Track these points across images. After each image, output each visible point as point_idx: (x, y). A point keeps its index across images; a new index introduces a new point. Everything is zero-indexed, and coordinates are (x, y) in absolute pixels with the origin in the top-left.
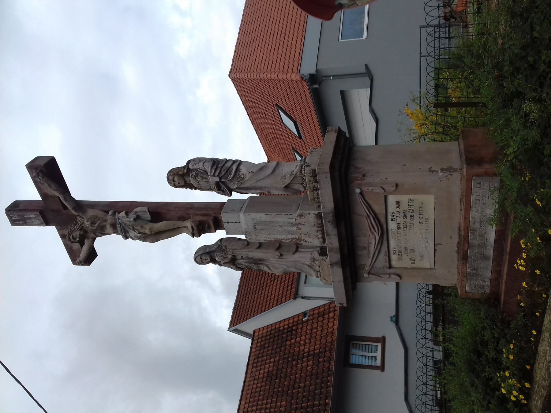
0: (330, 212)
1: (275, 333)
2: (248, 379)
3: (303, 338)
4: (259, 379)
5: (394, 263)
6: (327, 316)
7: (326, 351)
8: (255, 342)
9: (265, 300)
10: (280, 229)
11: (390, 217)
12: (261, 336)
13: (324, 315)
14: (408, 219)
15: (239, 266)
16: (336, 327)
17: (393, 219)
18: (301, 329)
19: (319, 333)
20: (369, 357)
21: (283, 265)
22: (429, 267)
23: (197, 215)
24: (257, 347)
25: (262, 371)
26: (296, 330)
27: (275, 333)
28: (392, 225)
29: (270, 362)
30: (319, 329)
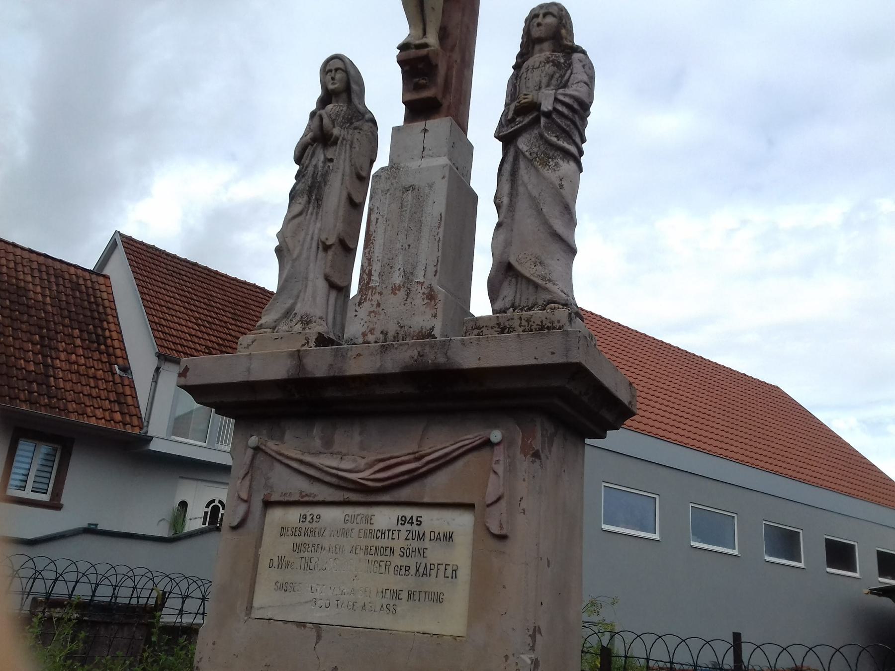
0: (448, 358)
1: (99, 313)
2: (18, 252)
3: (82, 361)
4: (16, 271)
5: (277, 515)
6: (117, 409)
7: (49, 397)
8: (87, 275)
9: (163, 303)
10: (399, 246)
11: (408, 512)
12: (97, 287)
13: (120, 403)
14: (397, 560)
15: (309, 151)
16: (93, 421)
17: (403, 520)
18: (100, 360)
19: (86, 390)
20: (26, 481)
21: (302, 249)
22: (256, 604)
23: (449, 68)
24: (78, 277)
25: (29, 278)
26: (98, 350)
27: (99, 313)
28: (385, 518)
29: (44, 296)
30: (94, 392)
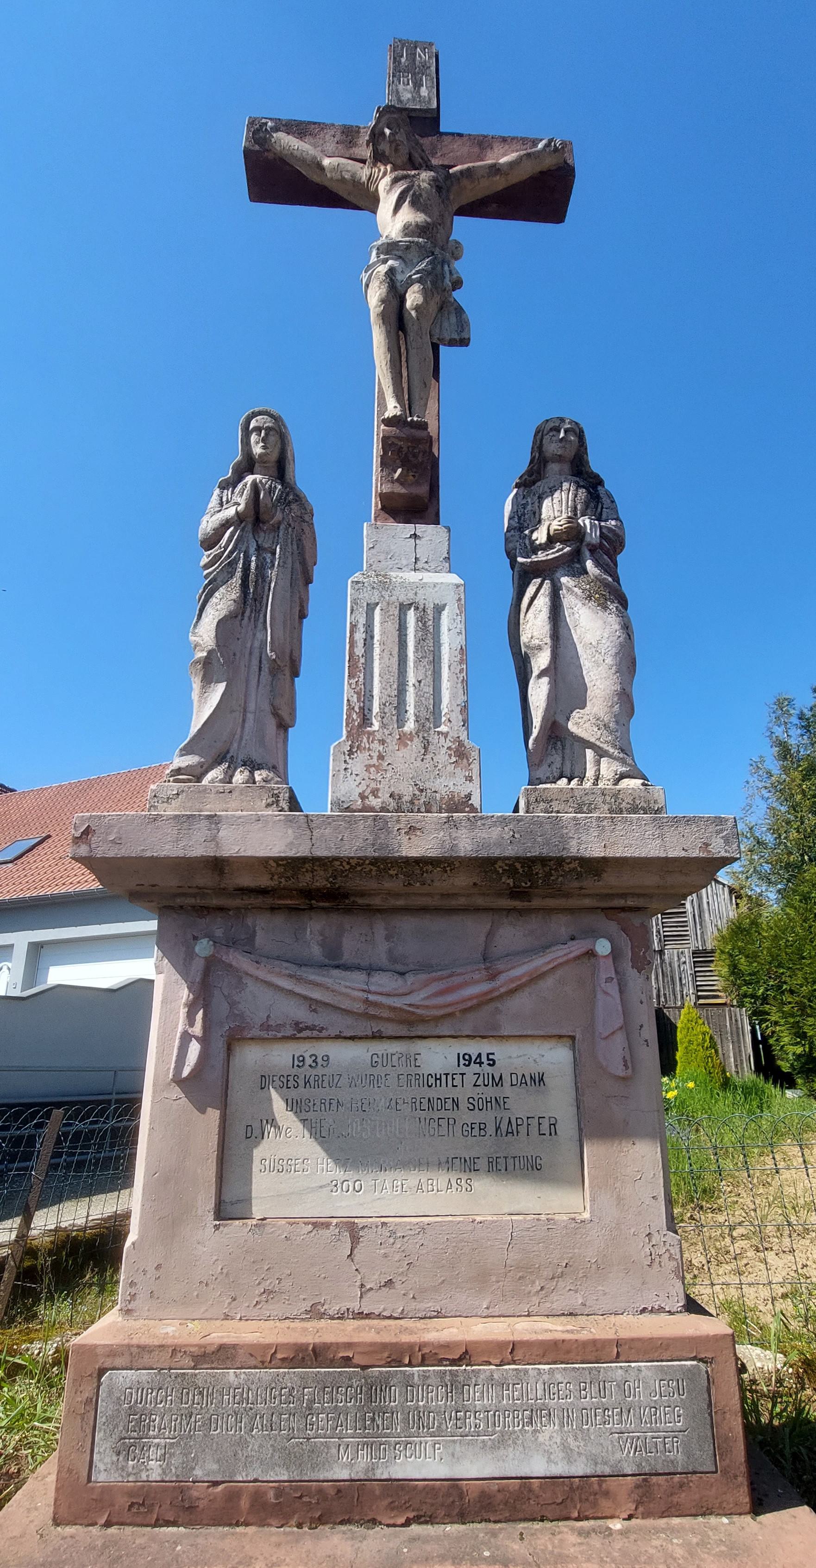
14: (465, 1116)
17: (468, 1060)
28: (437, 1056)
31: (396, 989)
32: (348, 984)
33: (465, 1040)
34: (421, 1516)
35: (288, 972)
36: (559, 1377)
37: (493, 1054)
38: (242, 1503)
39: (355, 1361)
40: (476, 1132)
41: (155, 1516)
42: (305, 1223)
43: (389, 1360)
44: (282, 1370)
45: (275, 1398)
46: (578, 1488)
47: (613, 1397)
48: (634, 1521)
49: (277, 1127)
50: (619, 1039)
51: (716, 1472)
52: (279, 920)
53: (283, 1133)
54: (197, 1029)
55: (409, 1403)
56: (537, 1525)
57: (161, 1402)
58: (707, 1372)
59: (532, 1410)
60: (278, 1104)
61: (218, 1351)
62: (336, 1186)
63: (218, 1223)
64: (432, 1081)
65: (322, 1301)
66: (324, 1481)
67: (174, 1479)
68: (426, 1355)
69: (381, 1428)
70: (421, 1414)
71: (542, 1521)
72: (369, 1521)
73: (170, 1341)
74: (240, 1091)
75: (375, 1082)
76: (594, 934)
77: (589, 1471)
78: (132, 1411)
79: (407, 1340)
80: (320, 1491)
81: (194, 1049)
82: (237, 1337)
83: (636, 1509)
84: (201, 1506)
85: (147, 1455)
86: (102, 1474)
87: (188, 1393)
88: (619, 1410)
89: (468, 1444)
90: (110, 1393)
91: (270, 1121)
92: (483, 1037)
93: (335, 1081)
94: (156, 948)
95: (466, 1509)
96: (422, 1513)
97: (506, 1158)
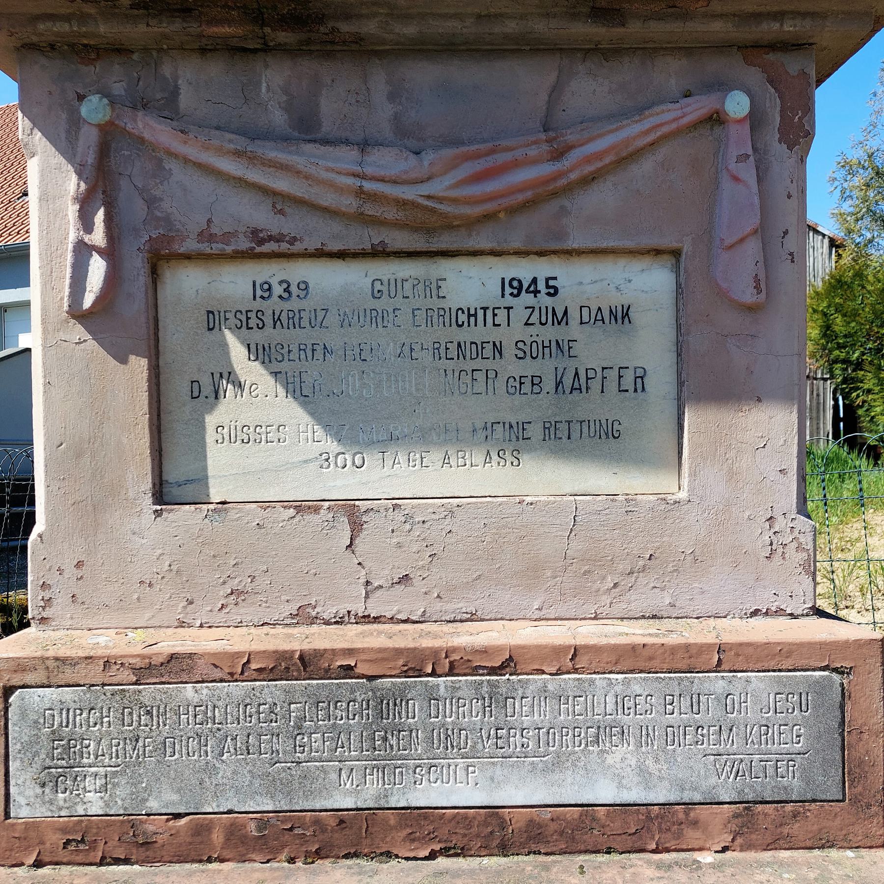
14: (511, 367)
17: (517, 287)
28: (471, 282)
31: (406, 172)
32: (330, 164)
33: (513, 259)
34: (450, 848)
35: (232, 146)
36: (637, 689)
37: (555, 278)
38: (214, 836)
39: (359, 670)
40: (527, 388)
41: (100, 854)
42: (285, 507)
43: (406, 668)
44: (258, 683)
45: (251, 716)
46: (657, 817)
47: (711, 713)
48: (729, 854)
49: (240, 386)
50: (752, 247)
51: (843, 800)
52: (215, 69)
53: (246, 390)
54: (98, 237)
55: (432, 720)
56: (601, 858)
57: (96, 724)
58: (842, 684)
59: (599, 727)
60: (237, 351)
61: (168, 662)
62: (327, 460)
63: (159, 508)
64: (462, 318)
65: (313, 603)
66: (321, 811)
67: (122, 812)
68: (455, 664)
69: (395, 748)
70: (450, 732)
71: (609, 853)
72: (382, 854)
73: (100, 653)
74: (177, 334)
75: (379, 320)
76: (723, 86)
77: (672, 798)
78: (55, 736)
79: (430, 645)
80: (317, 822)
81: (97, 268)
82: (194, 646)
83: (733, 840)
84: (160, 842)
85: (82, 786)
86: (23, 808)
87: (131, 714)
88: (717, 728)
89: (513, 766)
90: (23, 714)
91: (225, 375)
92: (541, 254)
93: (319, 319)
94: (20, 114)
95: (509, 840)
96: (449, 845)
97: (569, 422)
